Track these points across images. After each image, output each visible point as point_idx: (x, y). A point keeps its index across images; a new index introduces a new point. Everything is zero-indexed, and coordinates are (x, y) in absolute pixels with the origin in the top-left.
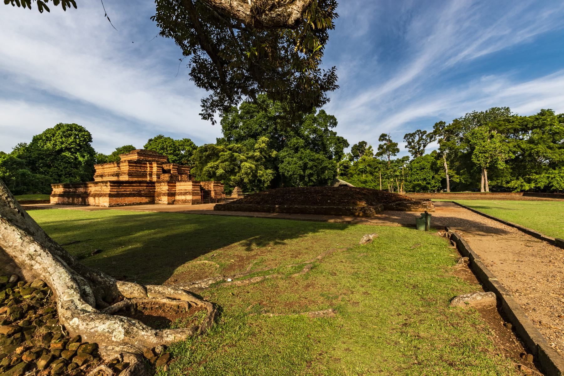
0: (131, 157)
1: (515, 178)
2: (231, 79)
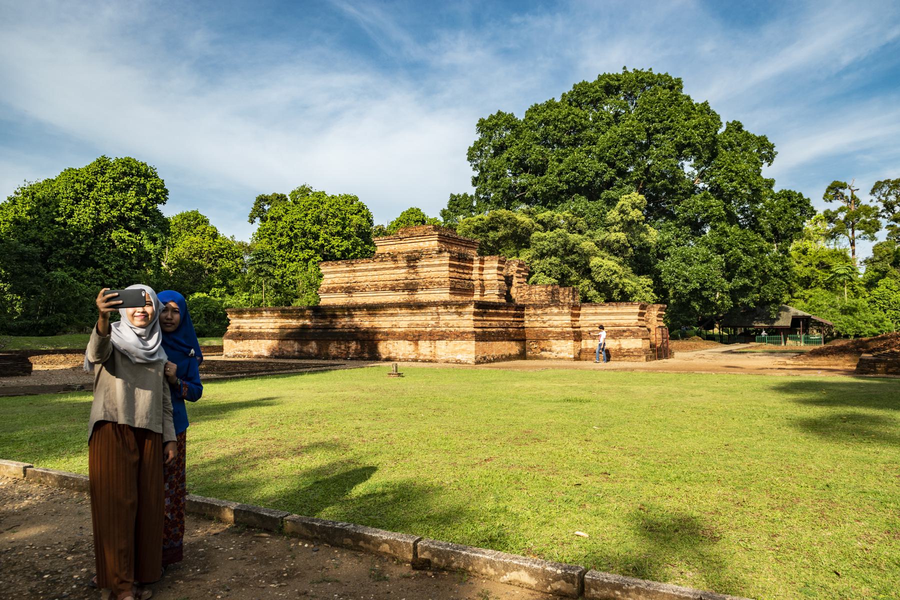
0: (393, 247)
1: (606, 298)
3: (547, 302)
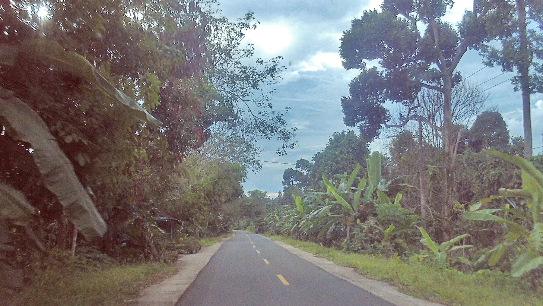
2: (321, 182)
3: (90, 303)
